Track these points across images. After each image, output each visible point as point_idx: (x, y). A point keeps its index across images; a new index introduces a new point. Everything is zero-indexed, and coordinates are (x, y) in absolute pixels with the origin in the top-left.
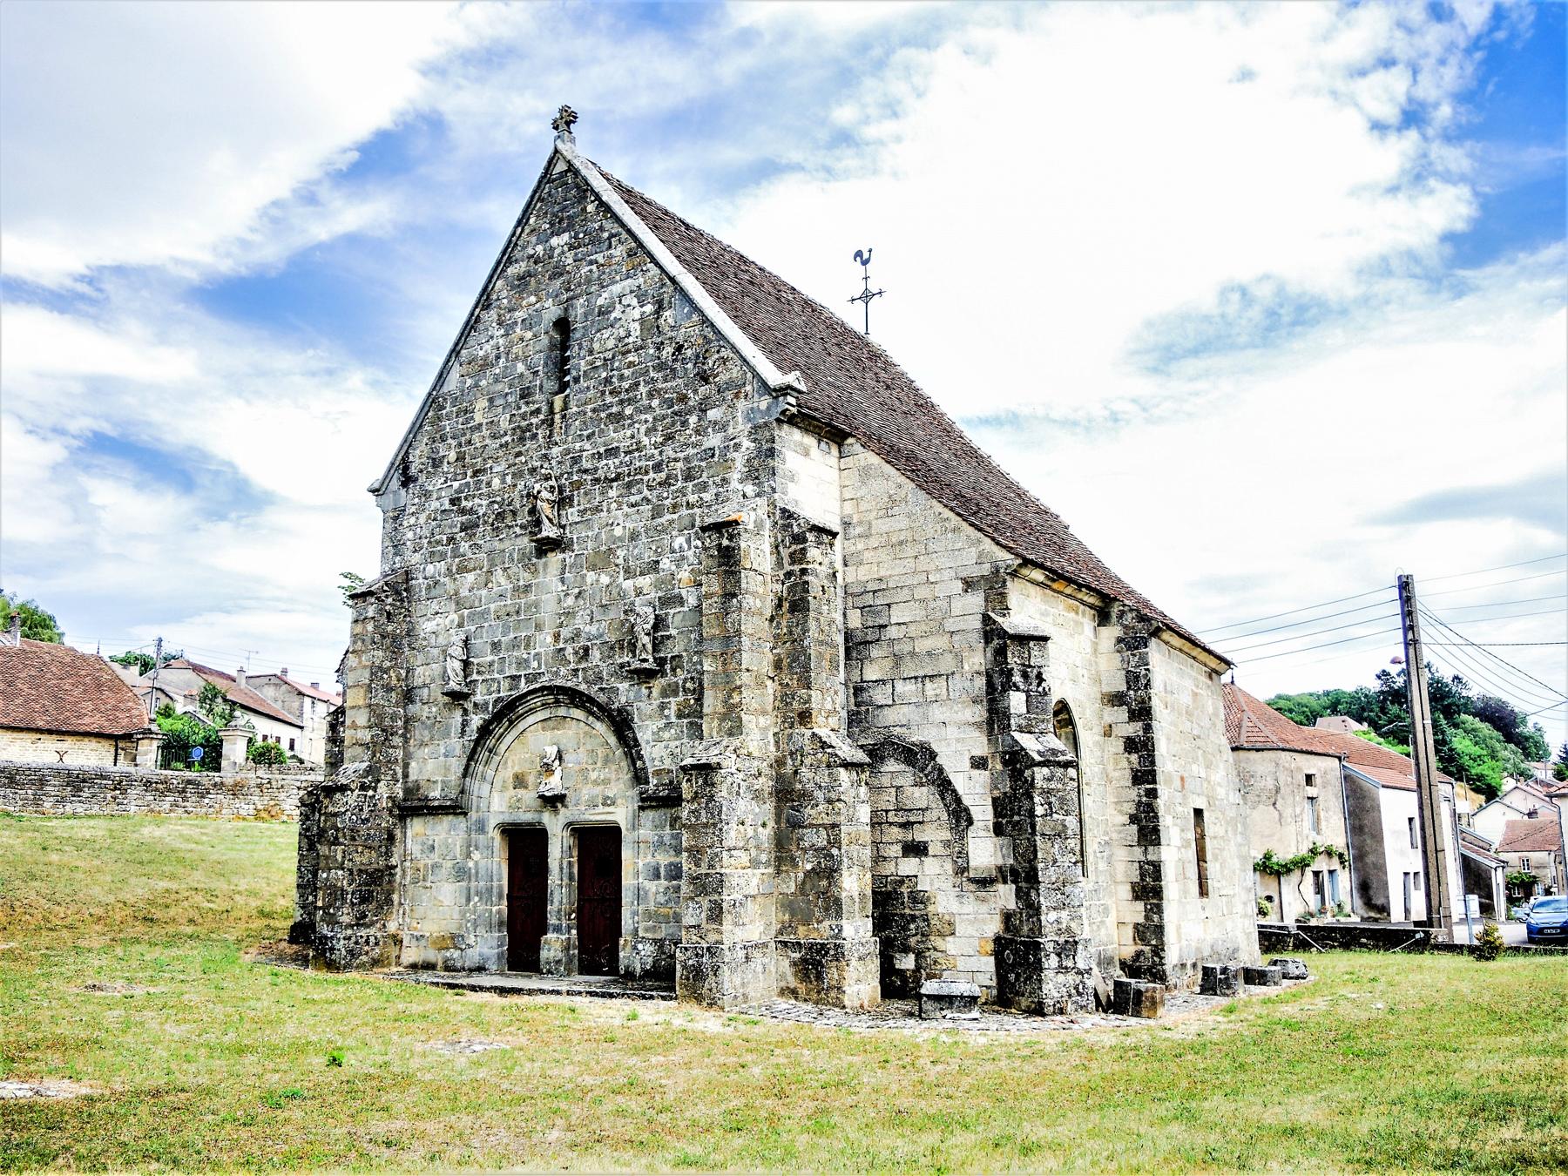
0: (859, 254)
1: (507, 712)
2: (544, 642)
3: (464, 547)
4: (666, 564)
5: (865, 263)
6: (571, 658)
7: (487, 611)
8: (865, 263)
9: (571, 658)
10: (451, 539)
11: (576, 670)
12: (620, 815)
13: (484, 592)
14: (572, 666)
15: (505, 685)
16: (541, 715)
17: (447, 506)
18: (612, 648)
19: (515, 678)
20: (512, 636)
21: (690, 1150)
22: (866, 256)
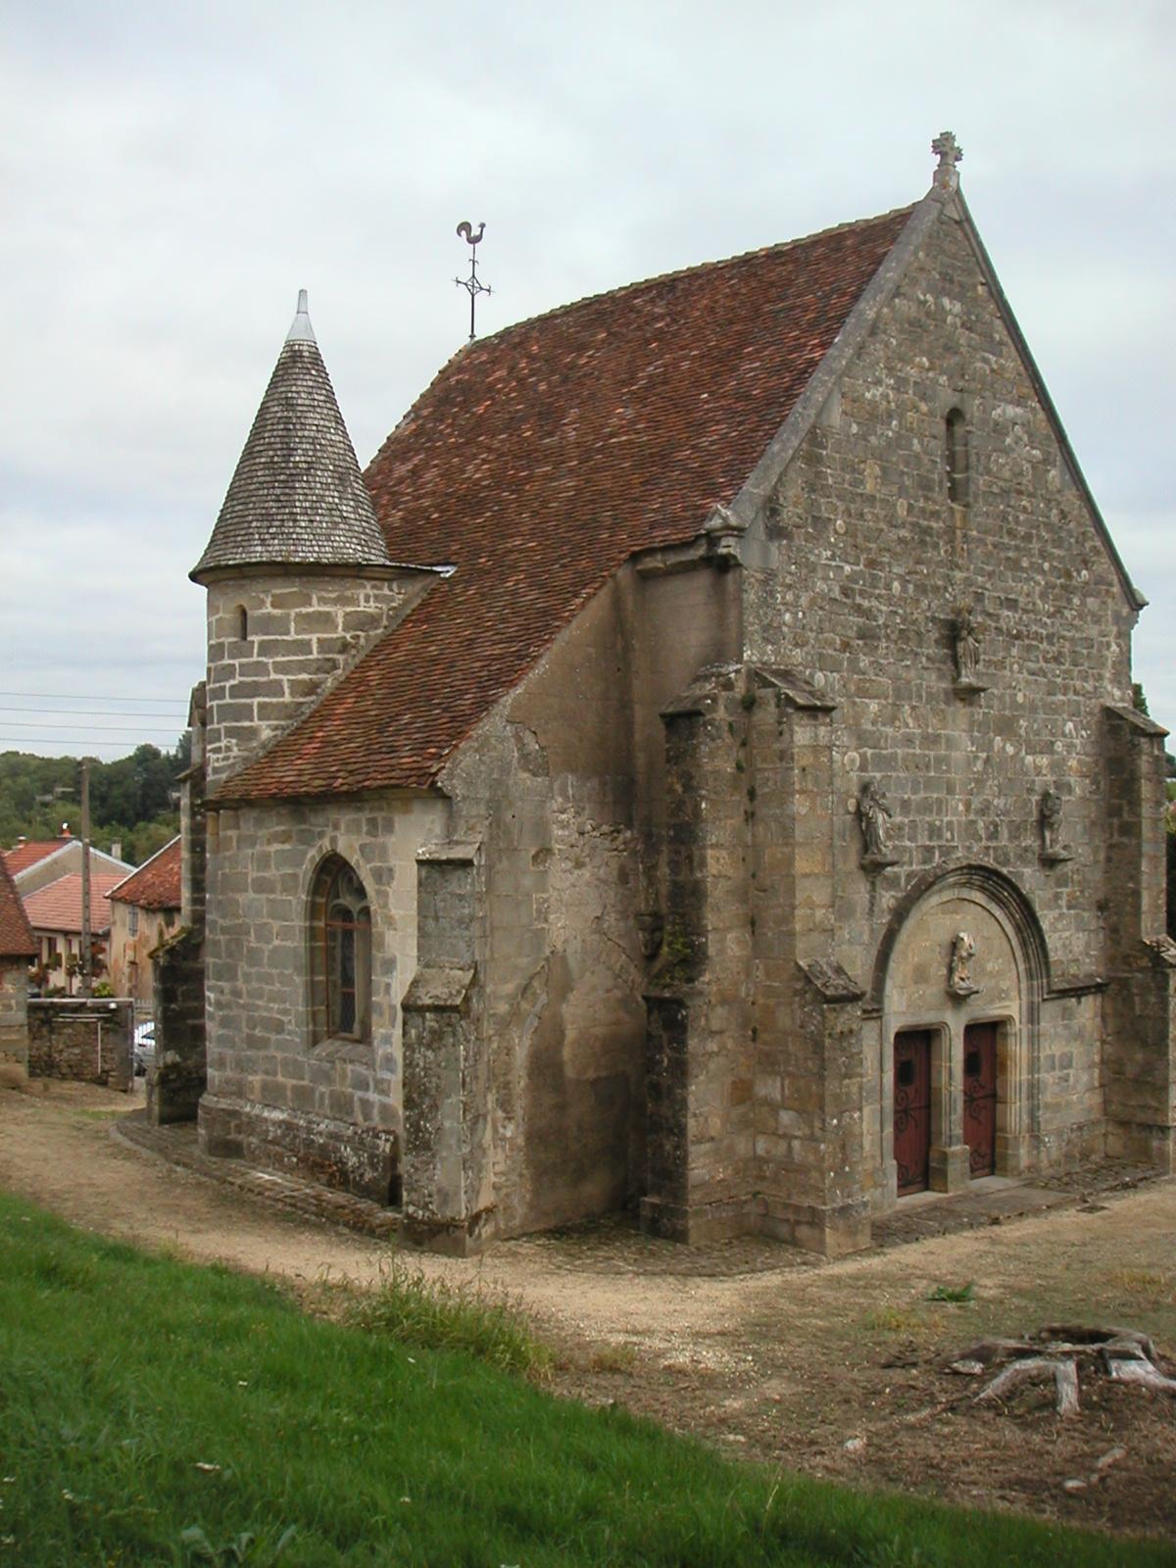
0: (465, 227)
1: (924, 886)
2: (956, 811)
3: (864, 662)
4: (1059, 746)
5: (474, 241)
6: (982, 833)
7: (894, 757)
8: (474, 241)
9: (982, 833)
10: (846, 646)
11: (987, 848)
12: (1012, 1008)
13: (889, 730)
14: (984, 843)
15: (917, 856)
16: (947, 896)
17: (836, 594)
18: (1018, 828)
19: (929, 850)
20: (922, 795)
21: (1152, 1346)
22: (475, 232)
